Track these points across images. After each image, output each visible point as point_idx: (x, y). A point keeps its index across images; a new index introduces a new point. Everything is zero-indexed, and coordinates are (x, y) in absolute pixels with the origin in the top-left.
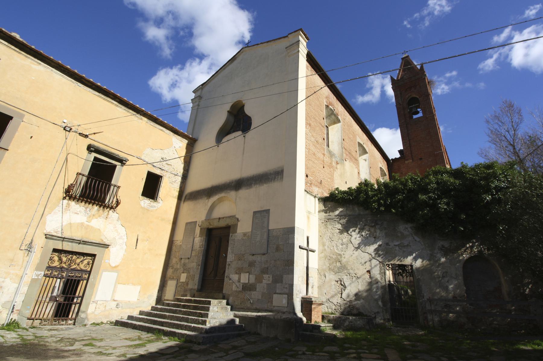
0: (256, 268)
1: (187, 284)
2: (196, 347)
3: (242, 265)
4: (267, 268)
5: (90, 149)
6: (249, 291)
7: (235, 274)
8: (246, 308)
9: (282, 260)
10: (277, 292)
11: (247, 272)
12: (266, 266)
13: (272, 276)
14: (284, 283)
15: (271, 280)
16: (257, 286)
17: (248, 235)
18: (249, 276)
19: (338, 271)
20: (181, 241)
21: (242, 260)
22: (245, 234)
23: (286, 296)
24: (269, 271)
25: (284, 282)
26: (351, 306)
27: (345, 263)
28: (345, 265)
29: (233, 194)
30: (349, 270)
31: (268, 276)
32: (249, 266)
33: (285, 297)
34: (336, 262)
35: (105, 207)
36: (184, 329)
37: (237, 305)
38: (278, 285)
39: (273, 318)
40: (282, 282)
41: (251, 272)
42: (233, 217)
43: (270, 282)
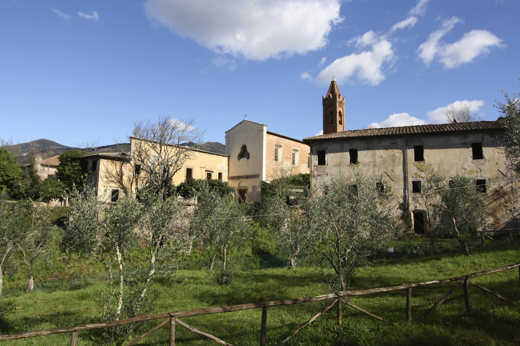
2: (166, 174)
5: (206, 171)
22: (250, 192)
29: (246, 180)
35: (334, 95)
42: (246, 187)
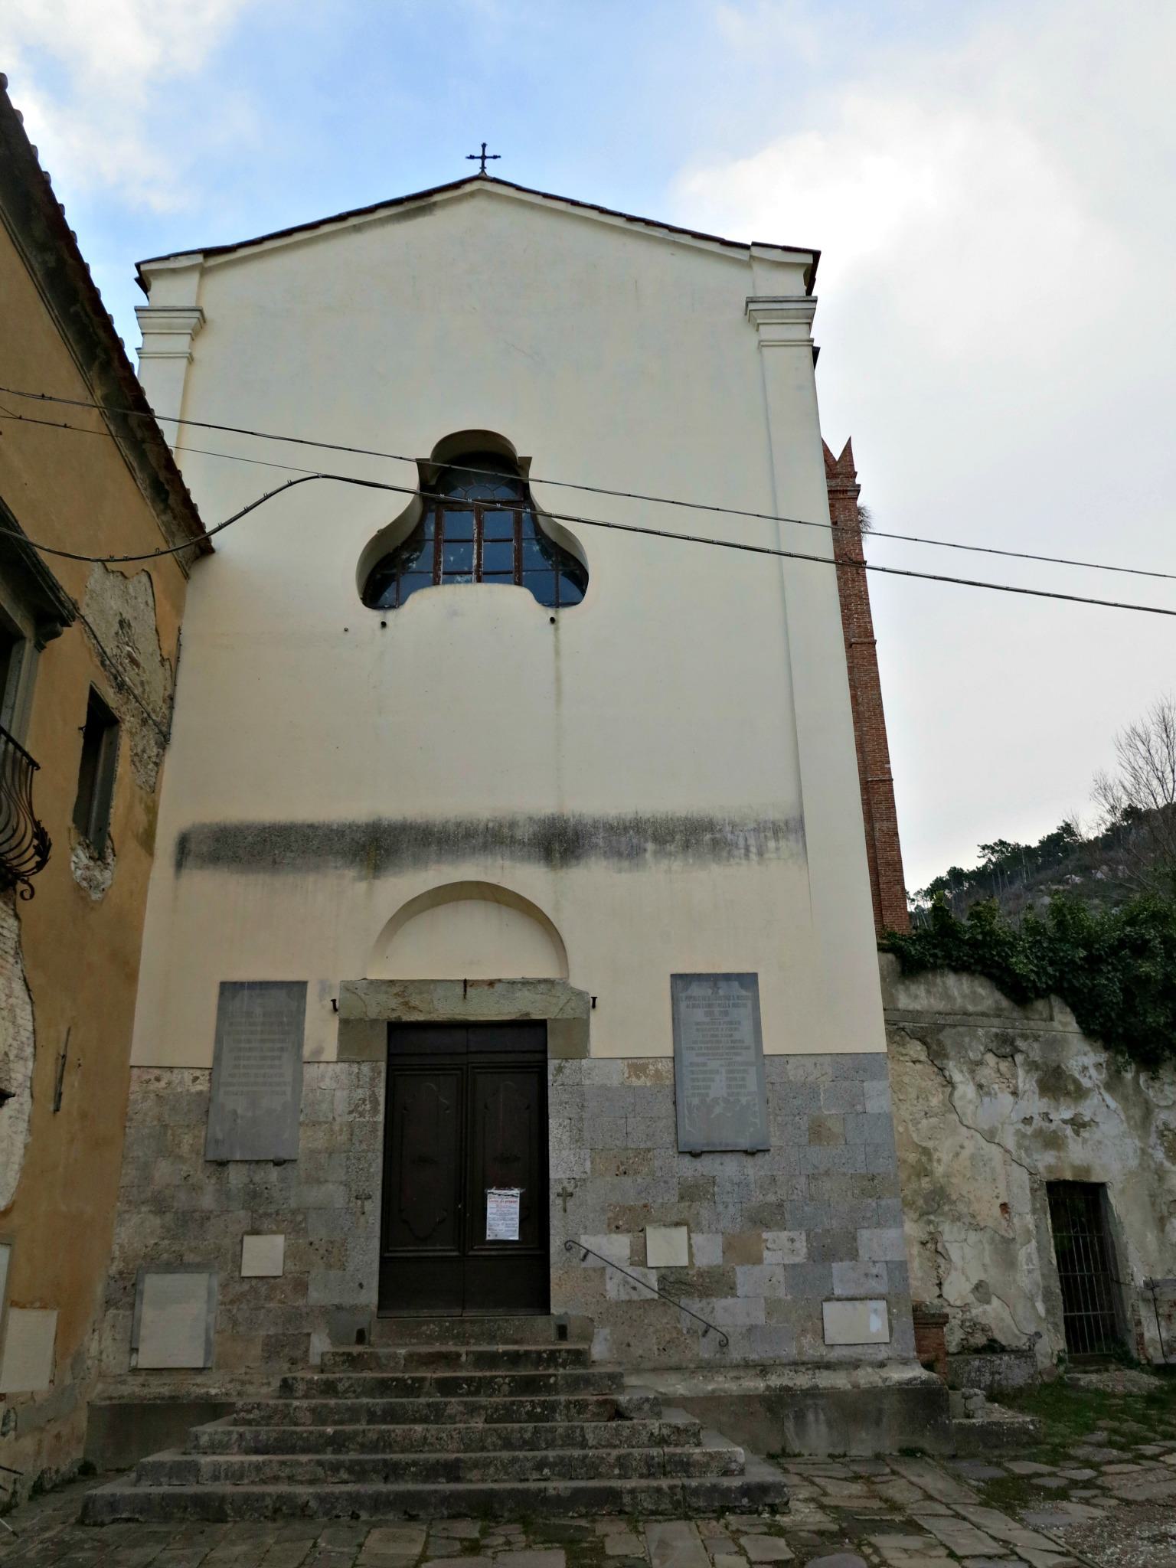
0: (720, 1208)
1: (301, 1286)
3: (643, 1195)
4: (780, 1206)
6: (697, 1299)
7: (611, 1231)
8: (692, 1366)
9: (844, 1174)
10: (838, 1292)
11: (677, 1224)
12: (771, 1198)
13: (808, 1236)
14: (867, 1259)
15: (805, 1250)
16: (739, 1274)
17: (657, 1070)
18: (689, 1238)
19: (924, 1206)
20: (198, 1073)
21: (636, 1172)
23: (882, 1305)
24: (787, 1216)
25: (864, 1254)
26: (968, 1324)
27: (941, 1180)
28: (942, 1187)
30: (955, 1202)
31: (785, 1234)
32: (682, 1198)
33: (875, 1311)
34: (918, 1176)
36: (617, 1471)
37: (641, 1357)
38: (836, 1267)
39: (849, 1387)
40: (853, 1255)
41: (698, 1224)
43: (800, 1259)
